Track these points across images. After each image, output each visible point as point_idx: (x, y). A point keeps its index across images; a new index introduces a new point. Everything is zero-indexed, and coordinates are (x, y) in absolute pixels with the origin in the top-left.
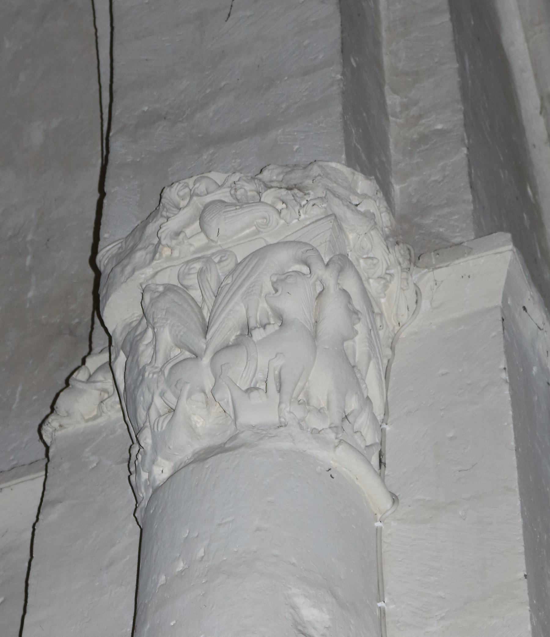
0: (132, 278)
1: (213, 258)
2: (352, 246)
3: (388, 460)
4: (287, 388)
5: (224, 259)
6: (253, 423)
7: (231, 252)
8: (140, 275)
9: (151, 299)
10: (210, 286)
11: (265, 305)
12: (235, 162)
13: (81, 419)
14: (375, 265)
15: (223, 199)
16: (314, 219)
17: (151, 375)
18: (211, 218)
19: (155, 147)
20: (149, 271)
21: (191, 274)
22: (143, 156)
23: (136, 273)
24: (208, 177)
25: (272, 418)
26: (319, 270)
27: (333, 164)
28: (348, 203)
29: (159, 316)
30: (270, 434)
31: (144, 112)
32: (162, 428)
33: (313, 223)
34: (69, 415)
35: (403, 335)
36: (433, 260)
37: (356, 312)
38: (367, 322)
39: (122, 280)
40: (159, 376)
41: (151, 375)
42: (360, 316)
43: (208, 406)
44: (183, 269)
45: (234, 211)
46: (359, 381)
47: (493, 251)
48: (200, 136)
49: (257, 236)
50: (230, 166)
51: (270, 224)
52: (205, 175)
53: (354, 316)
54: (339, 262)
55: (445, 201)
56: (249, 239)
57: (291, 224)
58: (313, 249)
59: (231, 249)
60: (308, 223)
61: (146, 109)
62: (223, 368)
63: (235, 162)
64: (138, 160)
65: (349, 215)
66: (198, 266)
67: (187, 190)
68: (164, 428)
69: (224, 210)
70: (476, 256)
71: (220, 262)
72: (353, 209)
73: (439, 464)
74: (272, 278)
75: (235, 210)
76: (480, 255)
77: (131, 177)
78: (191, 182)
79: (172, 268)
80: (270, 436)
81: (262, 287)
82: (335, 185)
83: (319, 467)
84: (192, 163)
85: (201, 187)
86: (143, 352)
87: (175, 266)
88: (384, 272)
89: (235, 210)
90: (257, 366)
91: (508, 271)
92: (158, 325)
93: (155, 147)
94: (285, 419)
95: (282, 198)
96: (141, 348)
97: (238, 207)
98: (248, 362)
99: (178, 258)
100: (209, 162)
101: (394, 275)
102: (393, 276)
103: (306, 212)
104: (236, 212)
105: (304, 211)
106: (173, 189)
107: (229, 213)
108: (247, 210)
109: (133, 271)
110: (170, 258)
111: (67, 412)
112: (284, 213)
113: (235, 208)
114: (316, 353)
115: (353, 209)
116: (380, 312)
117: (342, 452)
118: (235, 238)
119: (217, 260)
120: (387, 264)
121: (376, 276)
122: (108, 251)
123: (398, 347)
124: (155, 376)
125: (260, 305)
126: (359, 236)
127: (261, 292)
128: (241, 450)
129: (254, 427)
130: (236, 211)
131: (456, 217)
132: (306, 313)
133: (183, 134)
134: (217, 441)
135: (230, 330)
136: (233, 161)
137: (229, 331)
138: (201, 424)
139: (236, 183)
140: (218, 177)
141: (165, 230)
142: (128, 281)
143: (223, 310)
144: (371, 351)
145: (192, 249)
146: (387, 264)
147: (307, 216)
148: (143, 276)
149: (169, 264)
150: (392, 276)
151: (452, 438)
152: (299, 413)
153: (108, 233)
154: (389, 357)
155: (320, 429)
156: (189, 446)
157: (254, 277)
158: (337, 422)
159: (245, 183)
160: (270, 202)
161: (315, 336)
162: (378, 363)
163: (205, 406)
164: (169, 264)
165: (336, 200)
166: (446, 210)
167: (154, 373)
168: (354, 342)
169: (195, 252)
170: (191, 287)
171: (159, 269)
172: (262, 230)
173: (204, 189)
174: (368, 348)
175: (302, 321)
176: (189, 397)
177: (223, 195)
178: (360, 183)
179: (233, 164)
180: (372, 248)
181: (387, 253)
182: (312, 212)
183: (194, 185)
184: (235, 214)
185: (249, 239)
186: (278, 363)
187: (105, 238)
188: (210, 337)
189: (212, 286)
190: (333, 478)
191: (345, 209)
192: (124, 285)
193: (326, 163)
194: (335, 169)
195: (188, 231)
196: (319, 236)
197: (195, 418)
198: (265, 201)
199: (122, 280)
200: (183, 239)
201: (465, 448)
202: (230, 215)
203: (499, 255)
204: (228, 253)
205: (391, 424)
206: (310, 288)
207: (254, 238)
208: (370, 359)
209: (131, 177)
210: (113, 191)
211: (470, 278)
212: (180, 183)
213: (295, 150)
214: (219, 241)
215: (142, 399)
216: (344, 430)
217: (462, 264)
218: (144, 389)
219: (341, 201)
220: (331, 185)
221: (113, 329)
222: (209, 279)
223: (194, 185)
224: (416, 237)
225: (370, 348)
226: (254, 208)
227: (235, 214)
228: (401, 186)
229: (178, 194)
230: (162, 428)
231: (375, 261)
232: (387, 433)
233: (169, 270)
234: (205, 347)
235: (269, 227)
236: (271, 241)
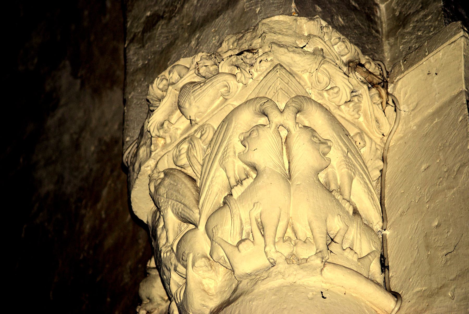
0: (140, 173)
1: (195, 135)
2: (309, 85)
3: (391, 262)
4: (269, 232)
5: (203, 133)
6: (249, 272)
7: (208, 124)
8: (146, 168)
9: (155, 187)
10: (197, 160)
11: (241, 163)
12: (215, 39)
13: (161, 301)
14: (337, 92)
15: (193, 80)
16: (265, 74)
17: (165, 255)
18: (184, 101)
19: (157, 46)
20: (151, 163)
21: (181, 154)
22: (149, 57)
23: (142, 168)
24: (178, 65)
25: (263, 262)
26: (276, 118)
27: (276, 18)
28: (294, 48)
29: (162, 201)
30: (263, 277)
31: (147, 17)
32: (180, 299)
33: (265, 77)
34: (150, 300)
35: (392, 144)
36: (402, 67)
37: (324, 142)
38: (340, 146)
39: (135, 177)
40: (171, 253)
41: (165, 255)
42: (329, 143)
43: (213, 267)
44: (175, 152)
45: (200, 89)
46: (340, 202)
47: (448, 43)
48: (189, 24)
49: (225, 104)
50: (211, 44)
51: (231, 91)
52: (176, 63)
53: (322, 147)
54: (293, 105)
55: (420, 6)
56: (220, 109)
57: (248, 84)
58: (269, 100)
59: (208, 123)
60: (262, 78)
61: (148, 14)
62: (214, 231)
63: (215, 39)
64: (146, 62)
65: (297, 58)
66: (185, 146)
67: (165, 82)
68: (182, 299)
69: (192, 91)
70: (435, 52)
71: (202, 135)
72: (301, 52)
73: (429, 253)
74: (240, 138)
75: (200, 88)
76: (438, 50)
77: (142, 79)
78: (166, 73)
79: (167, 154)
80: (263, 278)
81: (234, 148)
82: (280, 36)
83: (311, 293)
84: (184, 51)
85: (175, 76)
86: (160, 235)
87: (170, 151)
88: (349, 96)
89: (200, 88)
90: (241, 220)
91: (464, 55)
92: (162, 209)
93: (157, 46)
94: (273, 259)
95: (234, 64)
96: (159, 233)
97: (202, 84)
98: (233, 219)
99: (170, 144)
100: (196, 46)
101: (362, 95)
102: (361, 96)
103: (257, 70)
104: (201, 90)
105: (255, 70)
106: (154, 85)
107: (196, 92)
108: (209, 84)
109: (140, 167)
110: (165, 146)
111: (149, 299)
112: (239, 76)
113: (199, 86)
114: (290, 192)
115: (301, 52)
116: (359, 131)
117: (329, 272)
118: (209, 111)
119: (199, 136)
120: (349, 87)
121: (343, 102)
122: (129, 153)
123: (390, 156)
124: (168, 254)
125: (236, 165)
126: (311, 74)
127: (235, 153)
128: (240, 300)
129: (250, 275)
130: (201, 88)
131: (430, 17)
132: (274, 159)
133: (176, 27)
134: (226, 296)
135: (217, 194)
136: (214, 39)
137: (216, 196)
138: (213, 285)
139: (198, 63)
140: (183, 62)
141: (152, 124)
142: (138, 176)
143: (207, 179)
144: (350, 171)
145: (179, 132)
146: (349, 87)
147: (259, 73)
148: (149, 168)
149: (165, 151)
150: (359, 96)
151: (437, 226)
152: (286, 250)
153: (129, 136)
154: (381, 168)
155: (307, 257)
156: (205, 307)
157: (226, 142)
158: (322, 246)
159: (206, 61)
160: (227, 71)
161: (288, 177)
162: (363, 178)
163: (210, 268)
164: (165, 151)
165: (282, 50)
166: (422, 13)
167: (167, 253)
168: (333, 167)
169: (182, 135)
170: (185, 166)
171: (159, 158)
172: (226, 97)
173: (178, 76)
174: (347, 170)
175: (272, 168)
176: (193, 265)
177: (190, 77)
178: (305, 26)
179: (214, 42)
180: (330, 81)
181: (346, 79)
182: (262, 68)
183: (169, 75)
184: (200, 91)
185: (220, 109)
186: (256, 213)
187: (127, 142)
188: (201, 207)
189: (199, 161)
190: (325, 298)
191: (291, 54)
192: (137, 180)
193: (268, 20)
194: (277, 22)
195: (174, 119)
196: (271, 88)
197: (205, 282)
198: (223, 71)
199: (135, 177)
200: (168, 127)
201: (448, 232)
202: (197, 93)
203: (453, 45)
204: (206, 126)
205: (389, 229)
206: (272, 136)
207: (223, 106)
208: (351, 179)
209: (142, 79)
210: (130, 97)
211: (435, 73)
212: (158, 78)
213: (257, 12)
214: (196, 118)
215: (165, 277)
216: (331, 252)
217: (424, 63)
218: (164, 269)
219: (286, 49)
220: (275, 37)
221: (146, 221)
222: (195, 155)
223: (169, 75)
224: (401, 47)
225: (348, 169)
226: (213, 81)
227: (200, 91)
228: (386, 3)
229: (158, 88)
230: (180, 299)
231: (336, 90)
232: (387, 238)
233: (166, 156)
234: (199, 216)
235: (231, 93)
236: (237, 104)
